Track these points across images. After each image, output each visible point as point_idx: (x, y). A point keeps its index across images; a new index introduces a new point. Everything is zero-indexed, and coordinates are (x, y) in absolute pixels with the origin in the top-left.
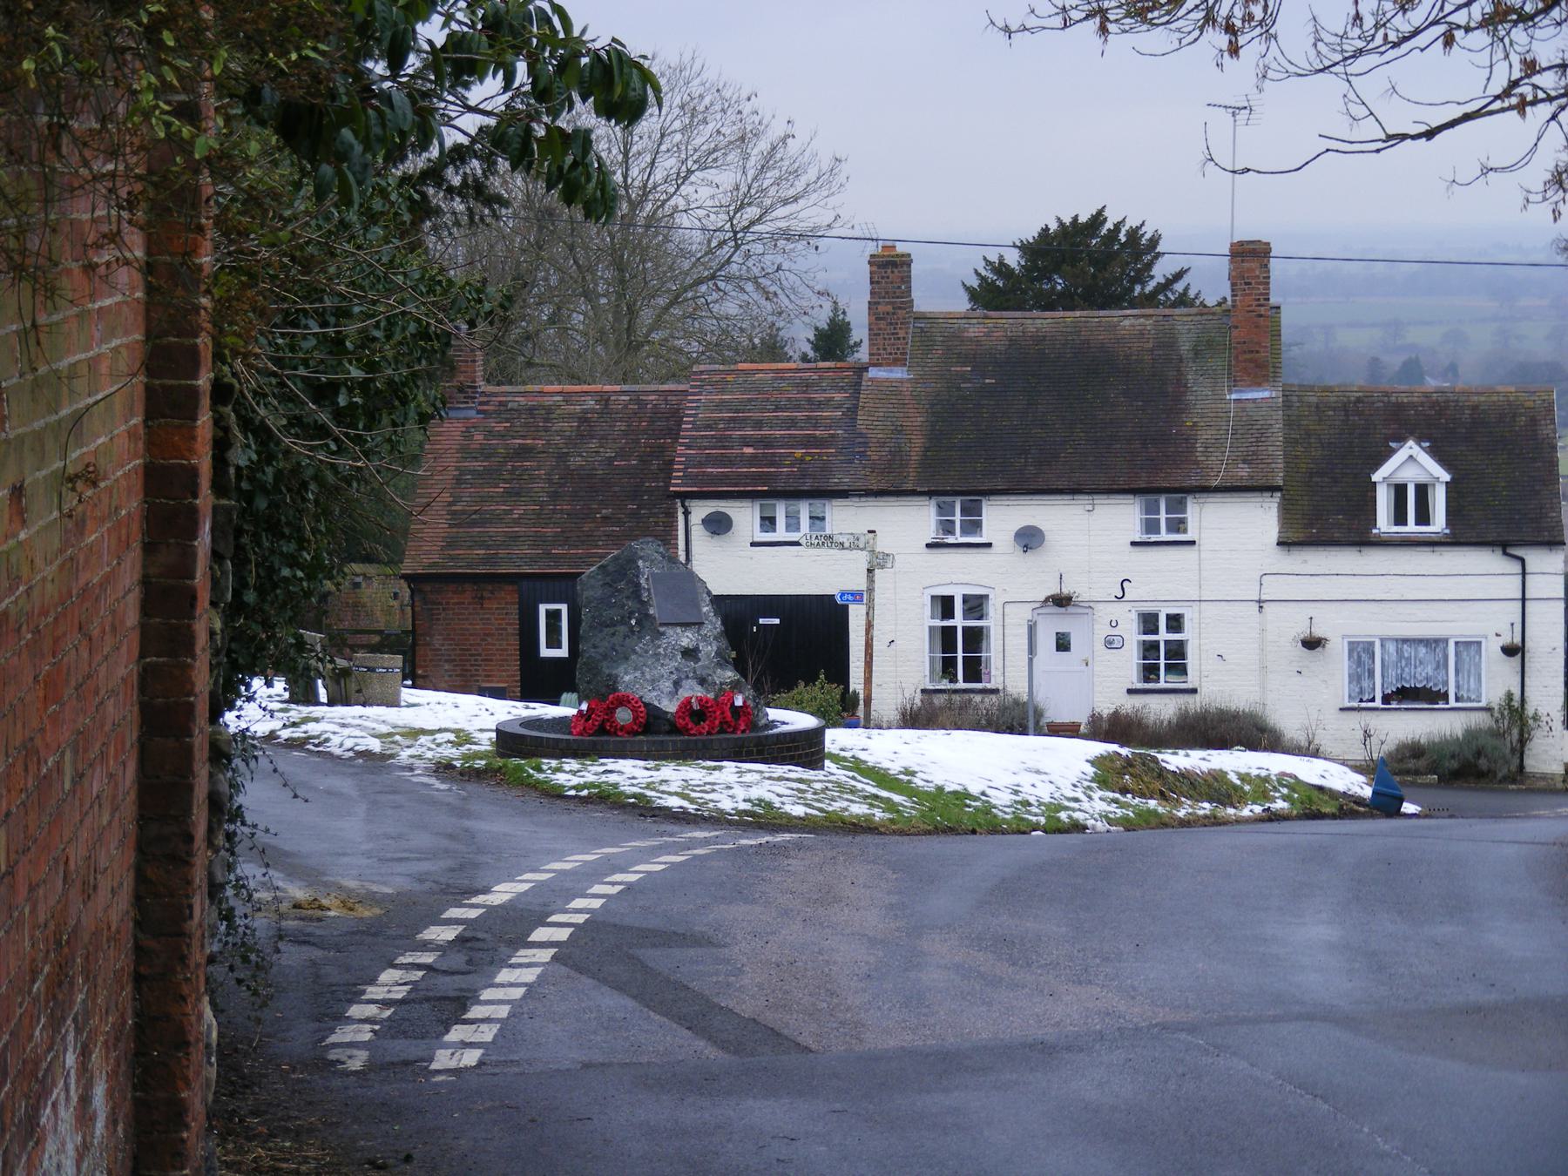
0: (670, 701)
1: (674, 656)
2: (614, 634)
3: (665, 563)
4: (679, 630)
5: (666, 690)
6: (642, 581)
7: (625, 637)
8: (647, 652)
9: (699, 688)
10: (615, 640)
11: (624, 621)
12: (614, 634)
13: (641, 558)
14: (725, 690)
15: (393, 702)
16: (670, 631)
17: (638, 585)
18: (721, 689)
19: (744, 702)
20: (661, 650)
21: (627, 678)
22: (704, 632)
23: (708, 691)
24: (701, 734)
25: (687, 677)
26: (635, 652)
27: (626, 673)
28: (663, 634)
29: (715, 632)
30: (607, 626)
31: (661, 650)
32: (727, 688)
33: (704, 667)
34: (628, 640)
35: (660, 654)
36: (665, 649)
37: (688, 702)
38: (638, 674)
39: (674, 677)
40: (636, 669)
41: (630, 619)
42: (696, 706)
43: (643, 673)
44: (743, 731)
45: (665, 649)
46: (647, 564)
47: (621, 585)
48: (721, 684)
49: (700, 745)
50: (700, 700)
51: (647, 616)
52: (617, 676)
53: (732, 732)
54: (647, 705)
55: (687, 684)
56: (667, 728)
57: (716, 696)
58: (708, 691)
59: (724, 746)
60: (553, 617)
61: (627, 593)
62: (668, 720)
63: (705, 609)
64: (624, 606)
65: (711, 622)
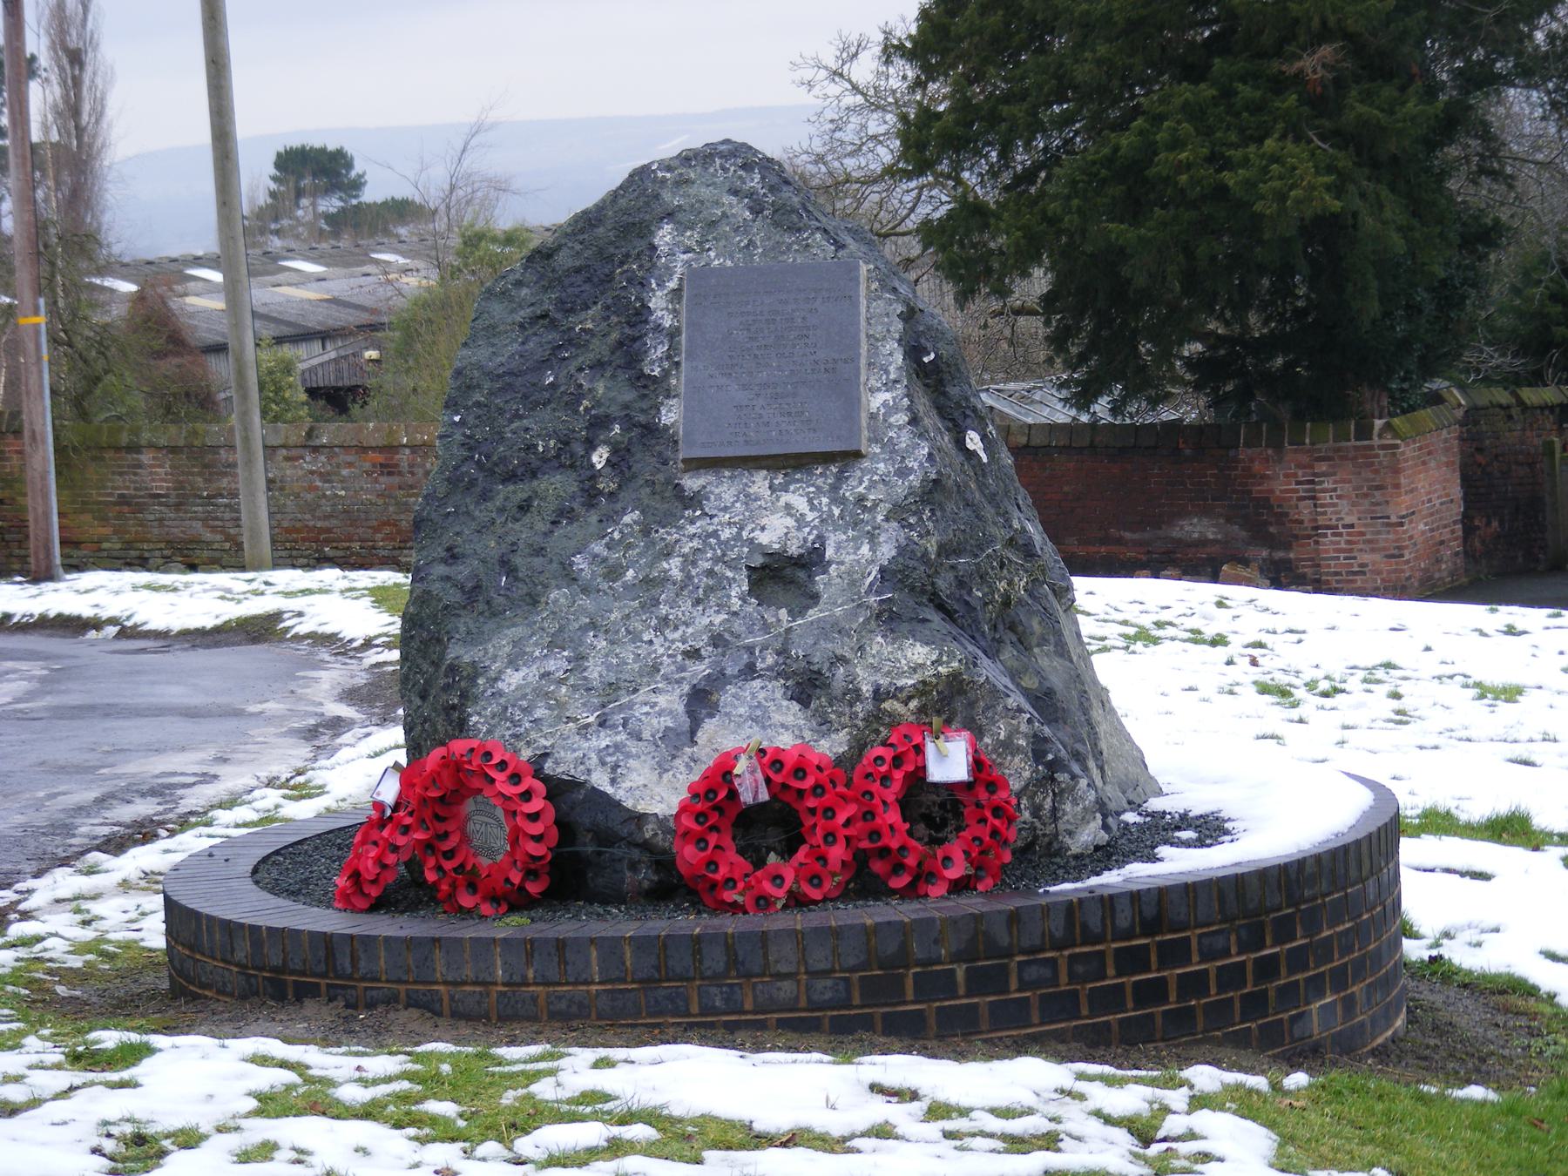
0: (662, 769)
1: (718, 585)
2: (524, 507)
3: (760, 231)
4: (760, 483)
5: (654, 725)
6: (658, 302)
7: (565, 514)
8: (614, 573)
9: (791, 713)
10: (524, 532)
11: (569, 457)
12: (524, 507)
13: (670, 215)
14: (894, 722)
15: (1154, 859)
16: (724, 490)
17: (641, 314)
18: (876, 717)
19: (978, 764)
20: (674, 567)
21: (513, 680)
22: (855, 487)
23: (825, 725)
24: (763, 903)
25: (750, 672)
26: (569, 576)
27: (513, 662)
28: (694, 500)
29: (900, 488)
30: (511, 477)
31: (674, 567)
32: (905, 711)
33: (834, 628)
34: (565, 528)
35: (665, 579)
36: (690, 561)
37: (722, 773)
38: (557, 664)
39: (701, 669)
40: (554, 645)
41: (591, 445)
42: (751, 787)
43: (579, 659)
44: (960, 886)
45: (690, 561)
46: (691, 237)
47: (587, 321)
48: (879, 695)
49: (715, 960)
50: (771, 761)
51: (651, 431)
52: (476, 670)
53: (912, 892)
54: (559, 789)
55: (738, 699)
56: (646, 876)
57: (859, 746)
58: (825, 725)
59: (819, 958)
60: (1281, 491)
61: (599, 348)
62: (646, 846)
63: (878, 400)
64: (579, 396)
65: (890, 447)
